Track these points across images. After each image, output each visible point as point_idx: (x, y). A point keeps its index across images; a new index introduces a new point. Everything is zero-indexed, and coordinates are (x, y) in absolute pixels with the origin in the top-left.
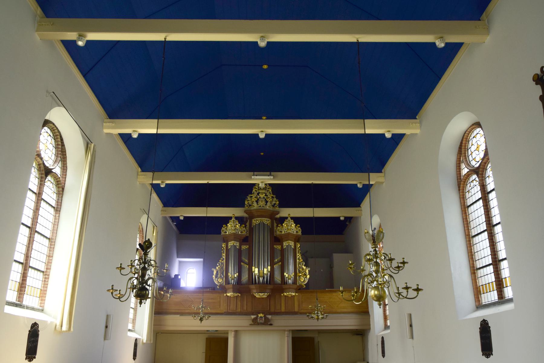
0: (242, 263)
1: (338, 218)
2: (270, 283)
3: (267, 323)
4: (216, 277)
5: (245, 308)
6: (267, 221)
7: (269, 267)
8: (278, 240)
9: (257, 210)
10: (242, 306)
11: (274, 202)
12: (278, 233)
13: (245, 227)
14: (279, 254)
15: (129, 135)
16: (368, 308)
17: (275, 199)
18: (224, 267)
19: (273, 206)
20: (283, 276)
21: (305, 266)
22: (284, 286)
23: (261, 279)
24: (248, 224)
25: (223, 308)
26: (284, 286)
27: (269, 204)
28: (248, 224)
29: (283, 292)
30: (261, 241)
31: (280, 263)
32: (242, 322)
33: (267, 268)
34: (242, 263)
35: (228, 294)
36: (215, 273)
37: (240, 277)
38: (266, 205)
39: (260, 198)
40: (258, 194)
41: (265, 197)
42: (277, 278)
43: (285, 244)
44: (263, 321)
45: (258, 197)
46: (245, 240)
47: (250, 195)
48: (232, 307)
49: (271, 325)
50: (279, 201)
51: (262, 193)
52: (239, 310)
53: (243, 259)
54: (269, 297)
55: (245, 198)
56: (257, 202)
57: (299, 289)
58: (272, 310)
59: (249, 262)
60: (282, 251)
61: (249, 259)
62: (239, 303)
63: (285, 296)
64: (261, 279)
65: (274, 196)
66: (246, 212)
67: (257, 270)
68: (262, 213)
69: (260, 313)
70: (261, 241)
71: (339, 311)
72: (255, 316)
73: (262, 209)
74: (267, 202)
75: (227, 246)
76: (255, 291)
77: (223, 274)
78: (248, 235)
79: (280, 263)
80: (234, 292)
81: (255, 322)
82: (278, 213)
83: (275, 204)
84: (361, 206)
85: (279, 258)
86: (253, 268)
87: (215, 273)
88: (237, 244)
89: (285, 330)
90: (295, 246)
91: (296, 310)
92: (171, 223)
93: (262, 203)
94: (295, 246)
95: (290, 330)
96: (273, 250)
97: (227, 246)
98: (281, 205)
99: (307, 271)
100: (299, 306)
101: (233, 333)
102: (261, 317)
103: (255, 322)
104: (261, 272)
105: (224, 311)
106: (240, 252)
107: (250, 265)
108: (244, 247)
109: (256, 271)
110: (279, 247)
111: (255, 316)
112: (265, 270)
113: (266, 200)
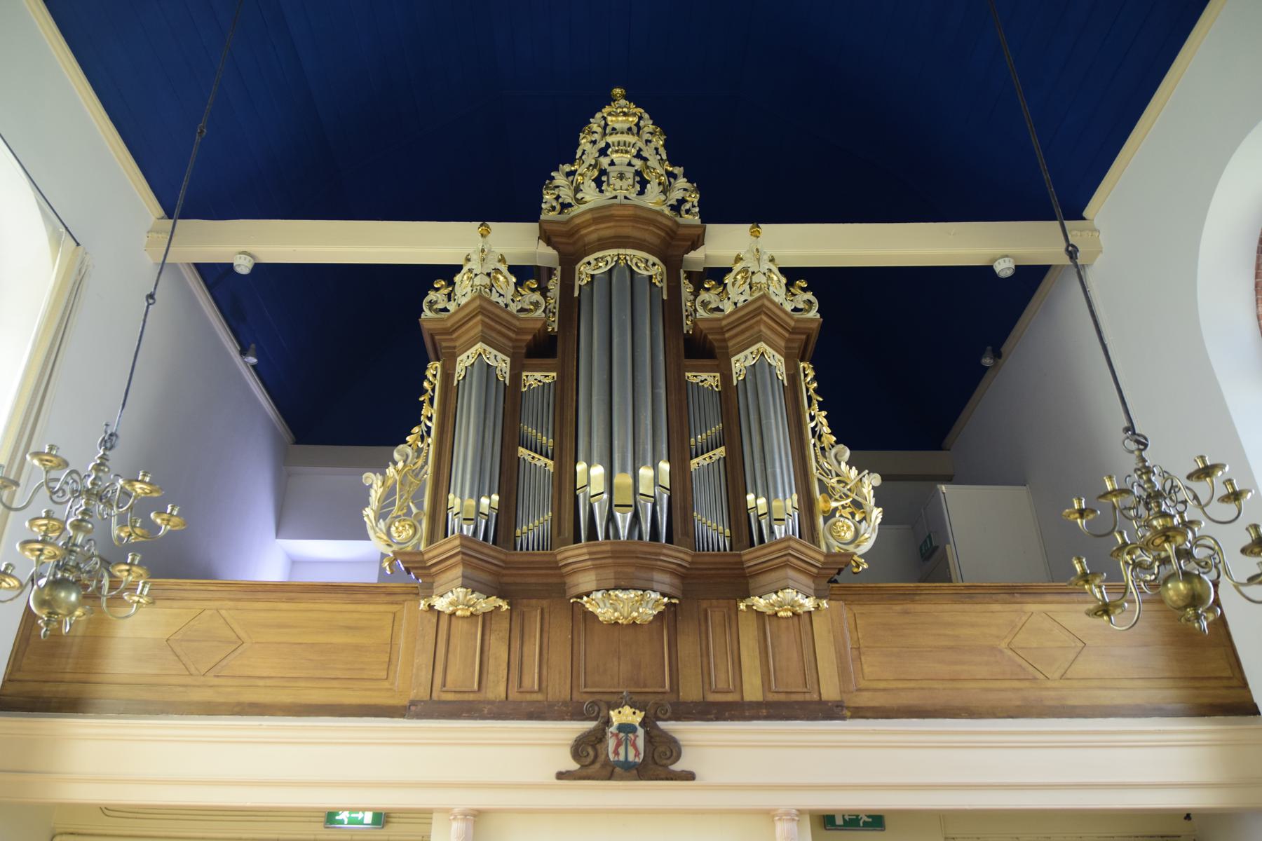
0: (523, 452)
1: (988, 270)
2: (670, 539)
3: (659, 761)
4: (382, 515)
5: (444, 344)
6: (648, 266)
7: (665, 466)
8: (702, 348)
9: (601, 215)
10: (515, 667)
11: (676, 195)
13: (544, 291)
14: (713, 409)
15: (227, 269)
16: (1244, 685)
17: (682, 182)
18: (429, 468)
19: (676, 208)
20: (738, 515)
21: (850, 463)
22: (750, 556)
23: (623, 520)
24: (554, 286)
25: (411, 679)
26: (750, 556)
27: (653, 189)
28: (554, 286)
29: (746, 595)
30: (621, 364)
31: (720, 452)
33: (655, 466)
34: (523, 452)
35: (441, 604)
36: (376, 493)
38: (641, 192)
39: (612, 163)
40: (603, 152)
41: (638, 163)
42: (711, 525)
43: (740, 363)
44: (635, 752)
45: (605, 162)
46: (540, 348)
47: (567, 168)
48: (461, 673)
49: (689, 776)
50: (699, 189)
51: (623, 148)
52: (496, 690)
53: (529, 430)
54: (669, 617)
55: (543, 178)
56: (598, 182)
57: (833, 577)
58: (691, 691)
59: (559, 444)
60: (728, 396)
61: (559, 435)
62: (498, 650)
63: (760, 614)
64: (623, 520)
65: (678, 170)
66: (547, 237)
67: (598, 471)
68: (623, 227)
69: (616, 705)
70: (621, 364)
71: (1076, 699)
72: (589, 725)
74: (644, 183)
75: (447, 376)
76: (586, 581)
77: (417, 498)
78: (554, 327)
79: (720, 452)
80: (469, 583)
81: (591, 760)
82: (697, 241)
83: (682, 201)
84: (1085, 214)
85: (715, 429)
87: (376, 493)
88: (502, 364)
89: (769, 815)
90: (793, 377)
91: (830, 691)
92: (237, 358)
93: (622, 189)
94: (793, 377)
95: (801, 812)
96: (679, 393)
97: (447, 376)
98: (715, 212)
99: (867, 490)
100: (843, 672)
101: (457, 827)
102: (626, 728)
103: (591, 760)
104: (623, 480)
105: (413, 695)
106: (511, 401)
107: (566, 455)
108: (534, 379)
109: (591, 475)
110: (710, 379)
111: (589, 725)
112: (646, 473)
113: (638, 173)
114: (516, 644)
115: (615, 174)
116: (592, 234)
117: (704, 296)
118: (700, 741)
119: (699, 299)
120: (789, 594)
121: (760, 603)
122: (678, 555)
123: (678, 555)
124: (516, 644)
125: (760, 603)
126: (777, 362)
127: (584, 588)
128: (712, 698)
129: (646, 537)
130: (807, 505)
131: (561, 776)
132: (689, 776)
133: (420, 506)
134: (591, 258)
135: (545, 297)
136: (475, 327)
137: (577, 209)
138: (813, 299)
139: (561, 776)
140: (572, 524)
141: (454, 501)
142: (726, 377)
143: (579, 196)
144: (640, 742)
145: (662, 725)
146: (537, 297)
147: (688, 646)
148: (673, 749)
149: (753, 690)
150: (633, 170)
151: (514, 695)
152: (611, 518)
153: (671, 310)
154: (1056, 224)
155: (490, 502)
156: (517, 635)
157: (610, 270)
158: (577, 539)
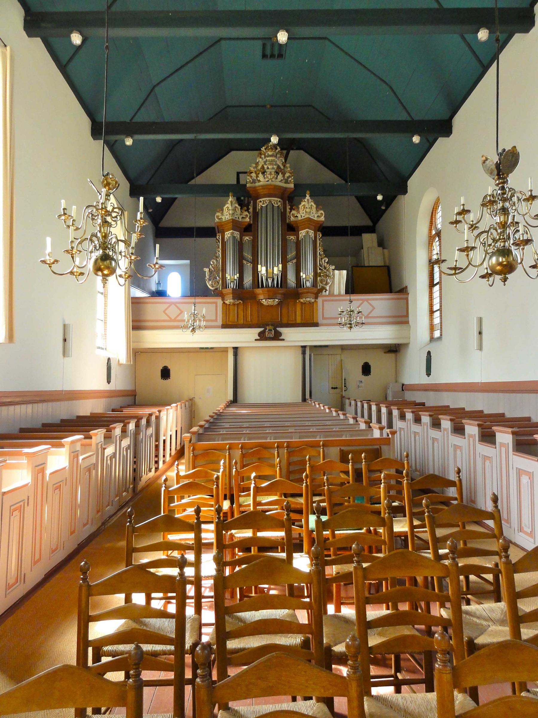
3: (277, 337)
7: (280, 266)
8: (291, 228)
12: (292, 219)
13: (248, 210)
26: (300, 290)
30: (269, 235)
31: (295, 261)
32: (246, 337)
34: (245, 262)
37: (241, 278)
39: (268, 168)
43: (302, 233)
44: (272, 334)
46: (248, 229)
48: (233, 318)
49: (283, 340)
52: (241, 322)
54: (280, 304)
58: (285, 321)
62: (241, 313)
63: (302, 303)
64: (270, 281)
67: (264, 269)
69: (268, 325)
70: (269, 235)
72: (262, 329)
73: (270, 185)
81: (262, 337)
83: (289, 177)
85: (294, 253)
86: (259, 266)
88: (237, 234)
90: (315, 237)
96: (285, 242)
103: (262, 337)
104: (270, 270)
106: (240, 246)
107: (255, 263)
108: (246, 238)
109: (262, 270)
111: (262, 329)
112: (276, 269)
114: (245, 310)
115: (268, 173)
116: (261, 192)
117: (293, 212)
118: (286, 332)
119: (292, 213)
120: (308, 299)
121: (302, 301)
122: (282, 291)
123: (282, 291)
124: (245, 310)
125: (302, 301)
126: (311, 233)
127: (261, 298)
128: (290, 322)
129: (275, 285)
130: (316, 275)
131: (256, 340)
132: (283, 340)
133: (219, 277)
134: (261, 200)
135: (249, 212)
136: (230, 225)
137: (257, 184)
138: (323, 212)
139: (256, 340)
140: (257, 282)
141: (228, 276)
142: (298, 238)
143: (258, 179)
144: (273, 333)
145: (277, 329)
146: (247, 213)
147: (284, 311)
148: (280, 334)
149: (299, 321)
150: (274, 170)
151: (245, 323)
152: (267, 280)
153: (283, 216)
154: (213, 621)
155: (236, 276)
156: (245, 310)
157: (267, 206)
158: (259, 287)
